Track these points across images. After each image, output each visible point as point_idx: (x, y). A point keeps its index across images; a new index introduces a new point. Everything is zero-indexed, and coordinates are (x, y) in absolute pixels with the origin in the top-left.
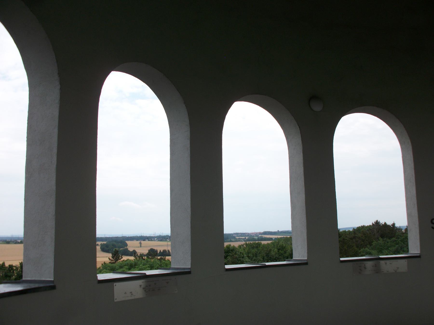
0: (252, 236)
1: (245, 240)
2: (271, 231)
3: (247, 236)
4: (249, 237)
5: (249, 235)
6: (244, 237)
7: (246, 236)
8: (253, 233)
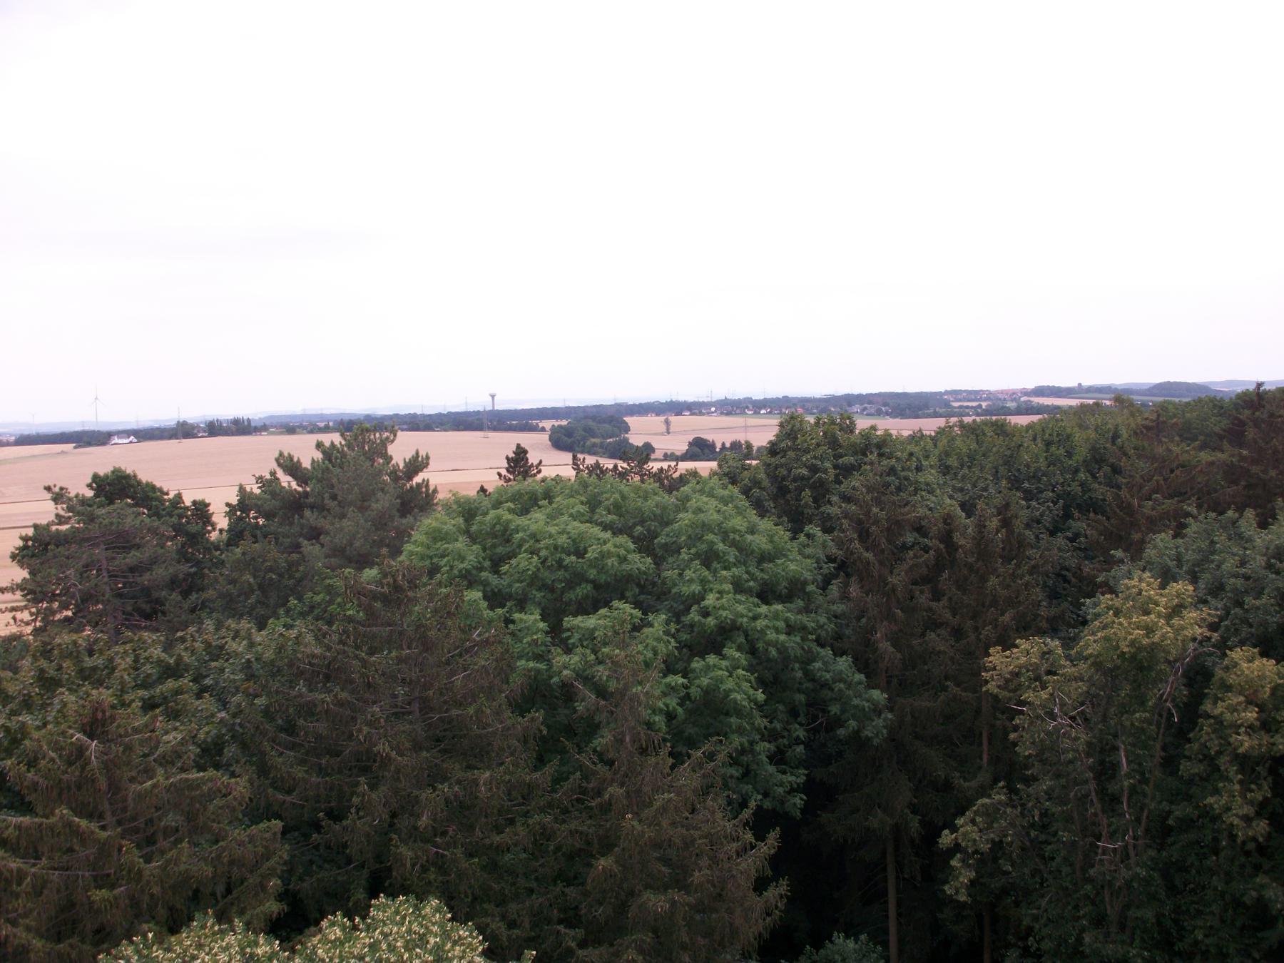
0: (1000, 399)
1: (979, 410)
2: (1057, 385)
3: (985, 400)
4: (990, 403)
5: (992, 397)
6: (974, 404)
7: (981, 400)
8: (1002, 392)
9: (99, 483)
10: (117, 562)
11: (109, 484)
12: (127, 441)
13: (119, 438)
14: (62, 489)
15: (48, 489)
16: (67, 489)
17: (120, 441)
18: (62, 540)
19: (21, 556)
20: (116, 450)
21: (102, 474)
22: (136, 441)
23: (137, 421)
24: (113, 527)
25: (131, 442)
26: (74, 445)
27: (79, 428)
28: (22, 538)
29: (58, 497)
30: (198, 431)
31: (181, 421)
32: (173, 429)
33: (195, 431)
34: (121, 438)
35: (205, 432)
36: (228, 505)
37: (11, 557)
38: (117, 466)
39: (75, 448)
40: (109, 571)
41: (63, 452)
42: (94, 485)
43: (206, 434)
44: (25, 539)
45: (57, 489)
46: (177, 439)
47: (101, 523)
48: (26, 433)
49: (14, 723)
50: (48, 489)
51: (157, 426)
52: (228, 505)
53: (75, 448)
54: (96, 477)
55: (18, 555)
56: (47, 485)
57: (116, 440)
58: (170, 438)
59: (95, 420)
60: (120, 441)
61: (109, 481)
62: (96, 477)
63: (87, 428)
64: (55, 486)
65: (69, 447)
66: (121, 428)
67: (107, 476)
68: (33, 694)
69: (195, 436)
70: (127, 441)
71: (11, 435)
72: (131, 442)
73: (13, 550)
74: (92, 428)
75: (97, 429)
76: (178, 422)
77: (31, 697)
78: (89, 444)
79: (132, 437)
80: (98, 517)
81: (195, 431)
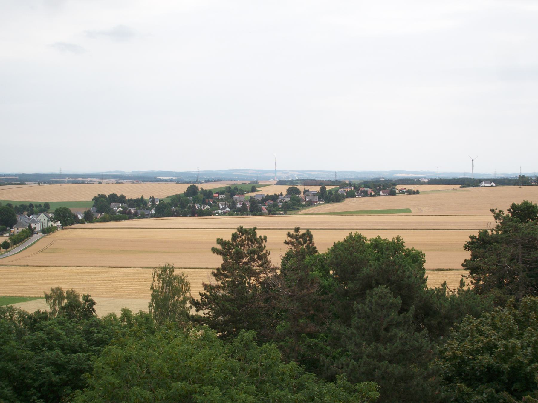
9: (514, 209)
10: (531, 256)
11: (521, 210)
12: (490, 185)
13: (485, 183)
14: (500, 211)
15: (492, 211)
16: (503, 212)
17: (486, 185)
18: (496, 239)
19: (469, 246)
20: (483, 190)
21: (516, 204)
22: (495, 185)
23: (495, 174)
24: (529, 235)
25: (492, 186)
26: (460, 185)
27: (462, 176)
28: (470, 237)
29: (497, 216)
30: (531, 182)
31: (521, 175)
32: (516, 180)
33: (530, 182)
34: (487, 183)
35: (535, 182)
36: (142, 197)
37: (464, 247)
38: (526, 200)
39: (461, 187)
40: (523, 260)
41: (454, 189)
42: (512, 210)
43: (536, 184)
44: (472, 237)
45: (497, 211)
46: (519, 185)
47: (523, 233)
48: (434, 178)
49: (510, 344)
50: (492, 211)
51: (506, 177)
52: (142, 197)
53: (461, 187)
54: (513, 206)
55: (468, 246)
56: (492, 209)
57: (483, 184)
58: (514, 185)
59: (471, 172)
60: (486, 185)
61: (522, 208)
62: (513, 206)
63: (467, 177)
64: (496, 209)
65: (457, 187)
66: (485, 177)
67: (521, 206)
68: (515, 328)
69: (529, 184)
70: (490, 185)
71: (425, 178)
72: (492, 186)
73: (466, 243)
74: (469, 177)
75: (365, 173)
76: (520, 176)
77: (513, 330)
78: (468, 186)
79: (493, 183)
80: (520, 229)
81: (530, 182)
